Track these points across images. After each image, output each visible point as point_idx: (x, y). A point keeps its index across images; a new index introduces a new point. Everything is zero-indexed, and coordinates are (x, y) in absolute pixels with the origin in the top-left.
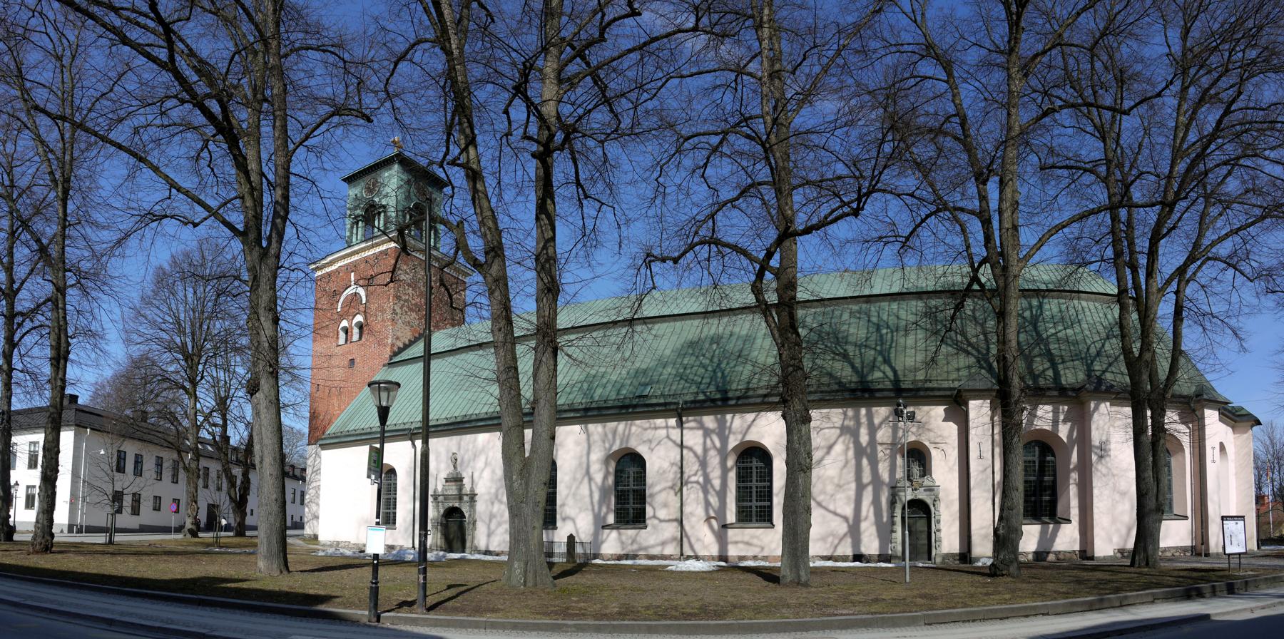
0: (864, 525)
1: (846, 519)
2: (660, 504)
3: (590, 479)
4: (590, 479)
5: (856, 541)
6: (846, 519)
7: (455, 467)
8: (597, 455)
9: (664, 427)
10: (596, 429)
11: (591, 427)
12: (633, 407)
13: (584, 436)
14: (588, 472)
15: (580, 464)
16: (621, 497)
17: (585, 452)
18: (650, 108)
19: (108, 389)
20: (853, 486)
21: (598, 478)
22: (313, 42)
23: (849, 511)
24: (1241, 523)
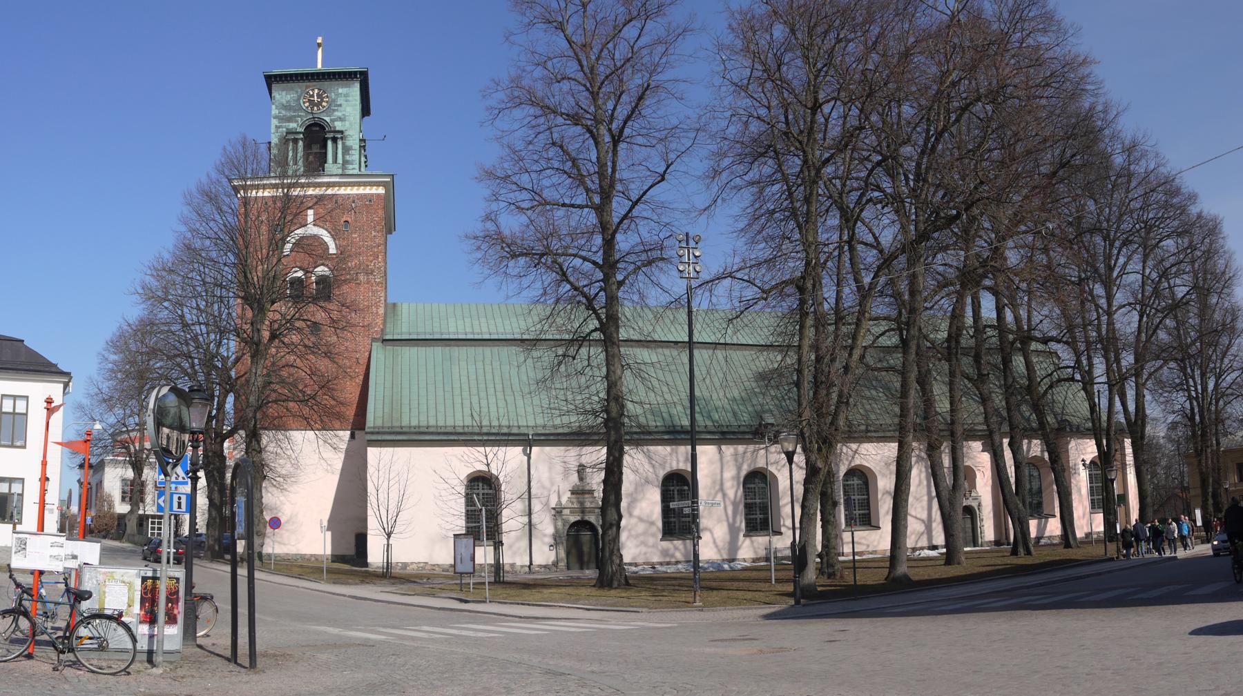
0: (934, 525)
1: (923, 521)
2: (787, 512)
3: (724, 495)
4: (724, 495)
5: (930, 538)
6: (923, 521)
7: (581, 479)
8: (729, 473)
9: (514, 454)
10: (728, 450)
11: (723, 447)
12: (690, 436)
13: (717, 457)
14: (722, 489)
15: (714, 482)
16: (749, 508)
17: (718, 471)
18: (738, 294)
19: (113, 357)
20: (926, 498)
21: (731, 493)
22: (655, 217)
23: (924, 516)
24: (34, 529)
